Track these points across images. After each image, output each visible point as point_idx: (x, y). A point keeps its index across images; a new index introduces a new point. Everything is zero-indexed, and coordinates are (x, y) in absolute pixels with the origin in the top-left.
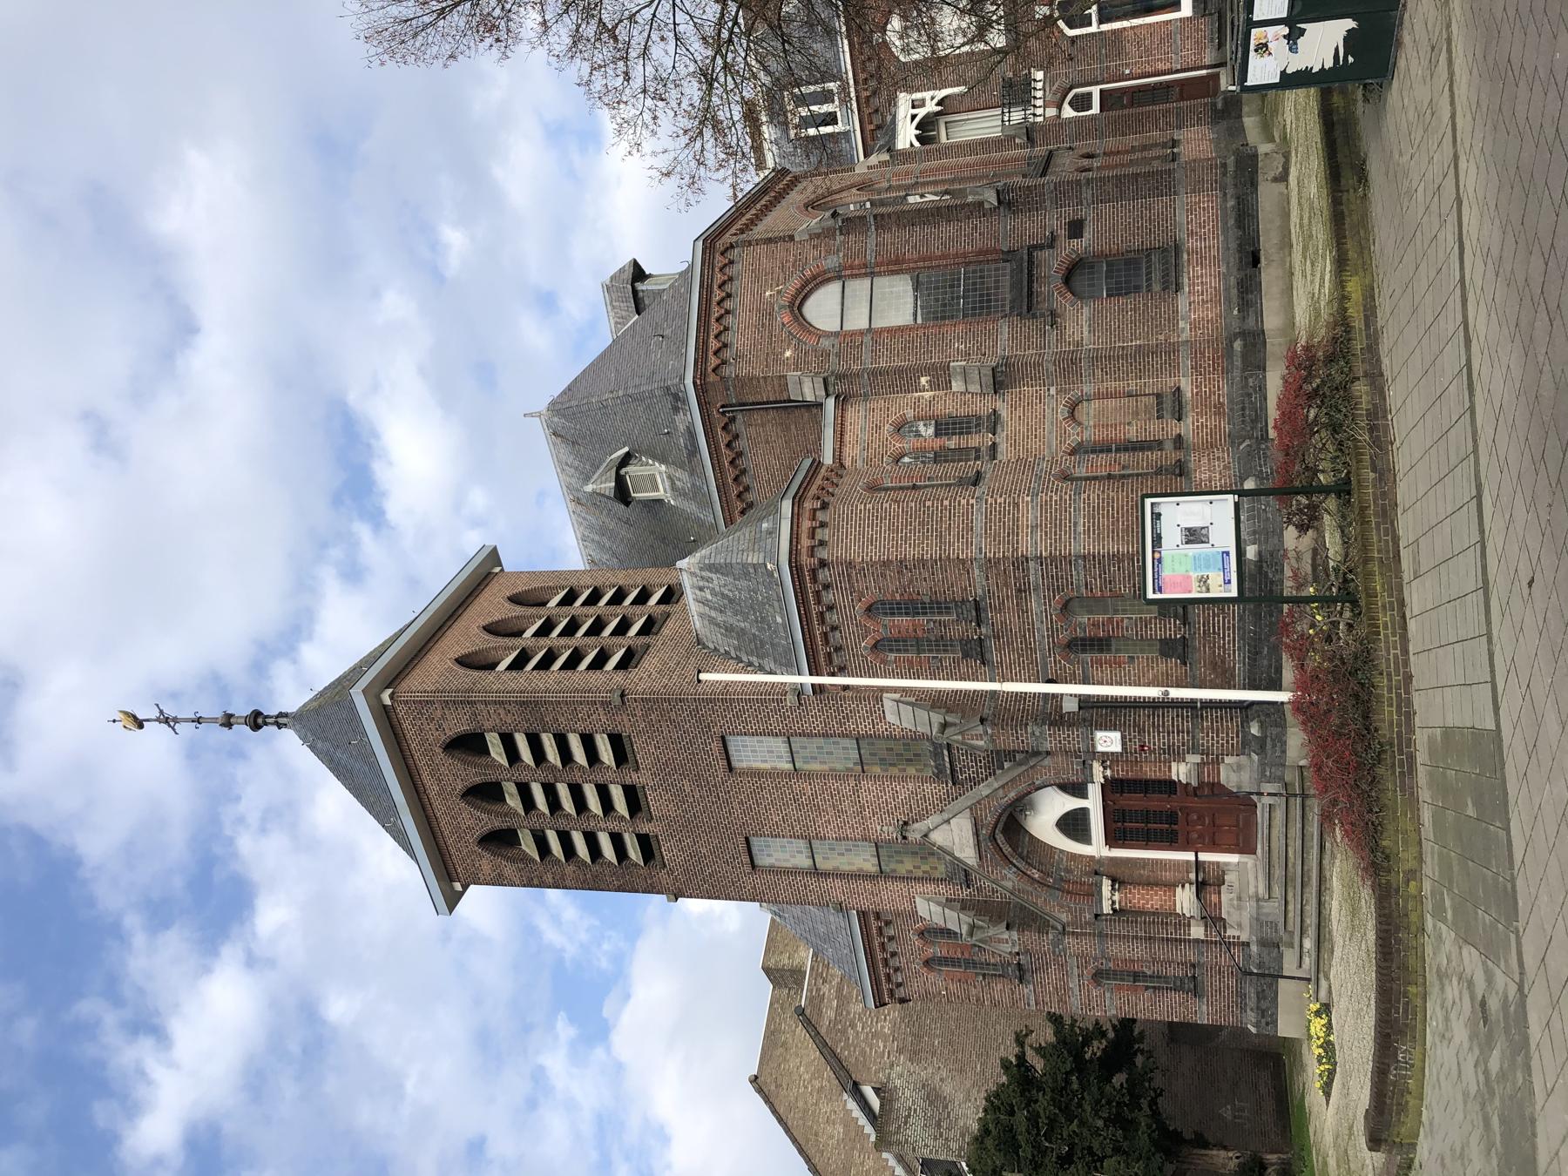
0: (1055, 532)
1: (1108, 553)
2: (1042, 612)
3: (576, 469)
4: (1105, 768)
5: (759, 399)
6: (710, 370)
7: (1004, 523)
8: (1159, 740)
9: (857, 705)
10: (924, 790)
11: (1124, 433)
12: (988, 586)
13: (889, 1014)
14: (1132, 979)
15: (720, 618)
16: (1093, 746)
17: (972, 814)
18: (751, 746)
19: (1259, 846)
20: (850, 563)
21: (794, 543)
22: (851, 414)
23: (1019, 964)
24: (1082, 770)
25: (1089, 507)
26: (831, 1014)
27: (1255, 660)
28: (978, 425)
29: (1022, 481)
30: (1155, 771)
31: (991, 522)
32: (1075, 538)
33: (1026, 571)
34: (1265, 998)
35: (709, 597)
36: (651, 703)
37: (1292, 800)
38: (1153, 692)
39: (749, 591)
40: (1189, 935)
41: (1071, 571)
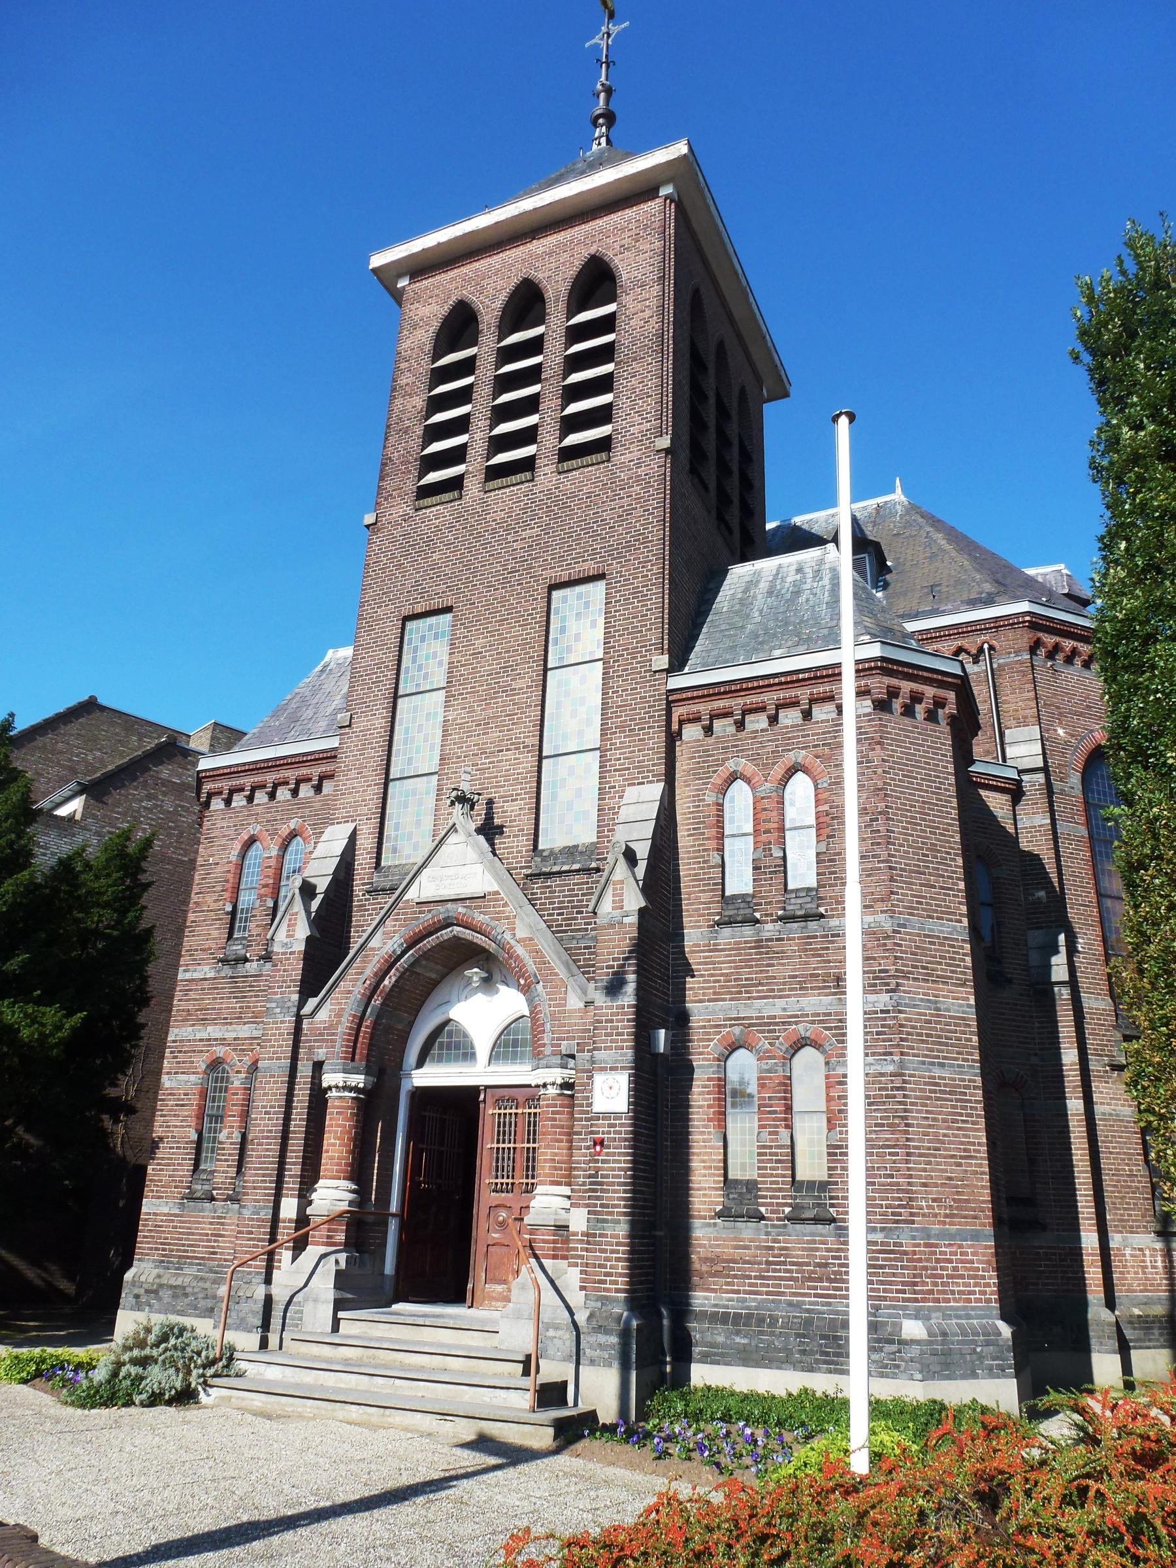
8: (613, 1169)
10: (517, 836)
17: (489, 894)
25: (965, 1087)
32: (923, 1063)
34: (175, 1296)
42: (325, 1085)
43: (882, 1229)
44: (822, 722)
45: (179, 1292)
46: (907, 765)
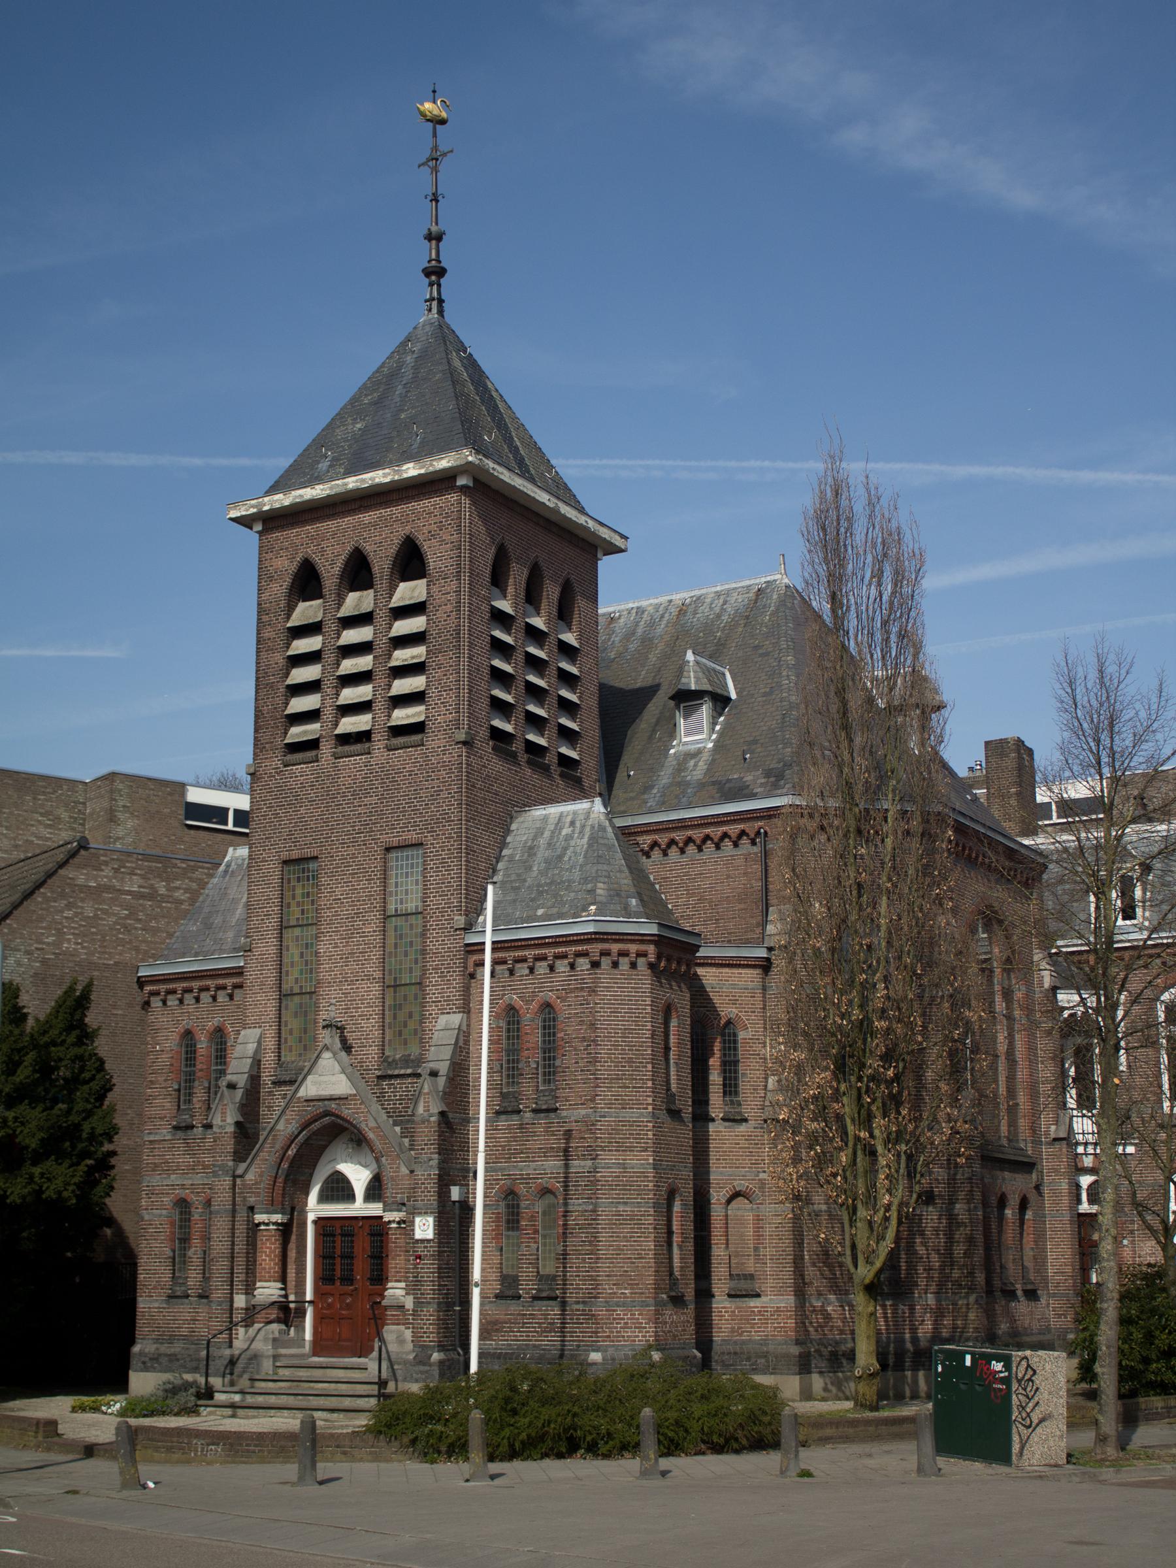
0: (619, 1185)
1: (598, 1233)
2: (544, 1170)
3: (719, 616)
4: (399, 1223)
7: (629, 1138)
8: (426, 1273)
9: (455, 988)
10: (371, 1046)
11: (717, 1244)
13: (83, 948)
15: (542, 842)
16: (420, 1214)
17: (351, 1095)
19: (321, 1359)
20: (594, 991)
22: (750, 976)
25: (641, 1215)
26: (81, 880)
27: (499, 1358)
28: (732, 1102)
29: (669, 1153)
30: (396, 1268)
31: (630, 1126)
32: (612, 1203)
33: (583, 1158)
34: (170, 1361)
35: (564, 832)
37: (376, 1387)
38: (476, 1274)
39: (569, 881)
40: (237, 1293)
41: (582, 1198)
42: (256, 1222)
44: (562, 972)
45: (173, 1358)
46: (614, 1004)
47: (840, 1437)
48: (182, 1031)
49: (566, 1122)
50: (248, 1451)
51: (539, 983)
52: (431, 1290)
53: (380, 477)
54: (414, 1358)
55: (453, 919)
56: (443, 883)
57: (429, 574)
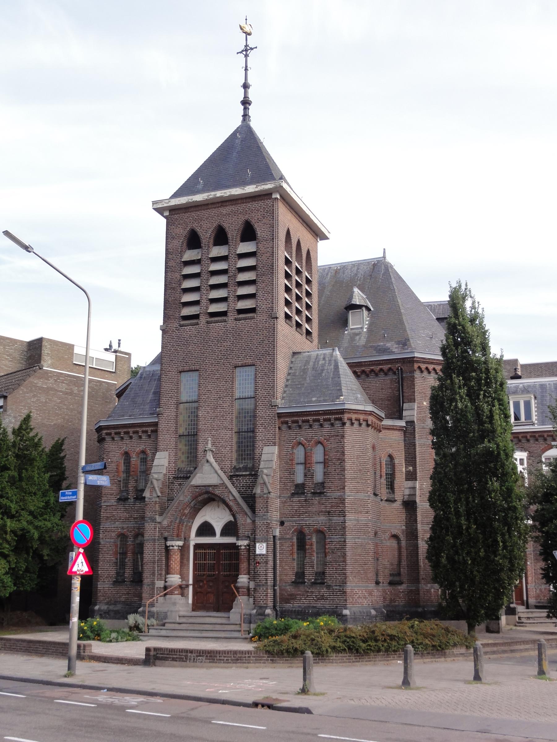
2: (318, 521)
3: (356, 275)
4: (245, 546)
5: (405, 388)
6: (420, 364)
8: (262, 570)
10: (226, 461)
12: (331, 499)
14: (121, 551)
17: (220, 484)
18: (248, 379)
21: (354, 411)
23: (129, 498)
24: (245, 536)
25: (366, 544)
26: (40, 384)
30: (244, 568)
32: (353, 538)
35: (320, 362)
36: (273, 331)
41: (338, 535)
43: (339, 585)
47: (492, 652)
48: (123, 452)
49: (329, 499)
50: (220, 660)
51: (315, 432)
52: (264, 579)
53: (236, 191)
54: (256, 612)
55: (271, 401)
56: (265, 384)
57: (258, 239)
